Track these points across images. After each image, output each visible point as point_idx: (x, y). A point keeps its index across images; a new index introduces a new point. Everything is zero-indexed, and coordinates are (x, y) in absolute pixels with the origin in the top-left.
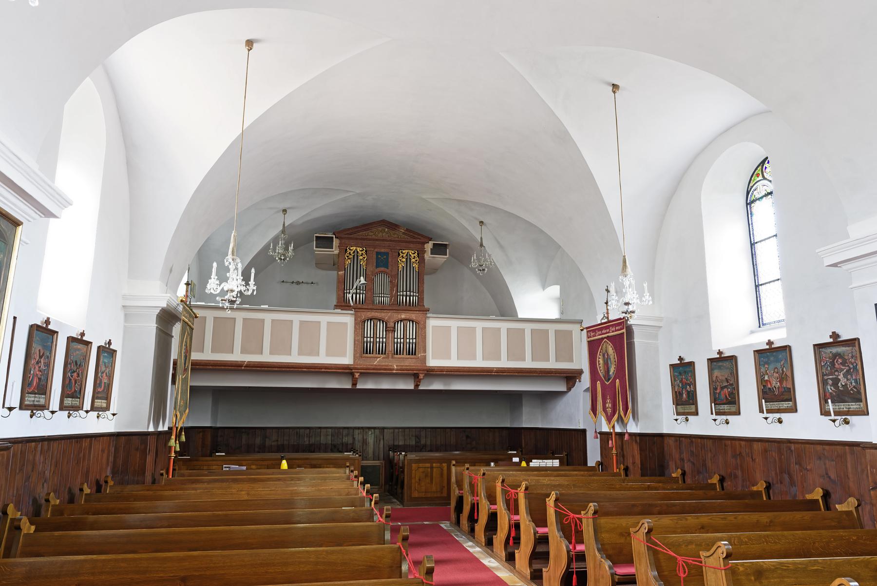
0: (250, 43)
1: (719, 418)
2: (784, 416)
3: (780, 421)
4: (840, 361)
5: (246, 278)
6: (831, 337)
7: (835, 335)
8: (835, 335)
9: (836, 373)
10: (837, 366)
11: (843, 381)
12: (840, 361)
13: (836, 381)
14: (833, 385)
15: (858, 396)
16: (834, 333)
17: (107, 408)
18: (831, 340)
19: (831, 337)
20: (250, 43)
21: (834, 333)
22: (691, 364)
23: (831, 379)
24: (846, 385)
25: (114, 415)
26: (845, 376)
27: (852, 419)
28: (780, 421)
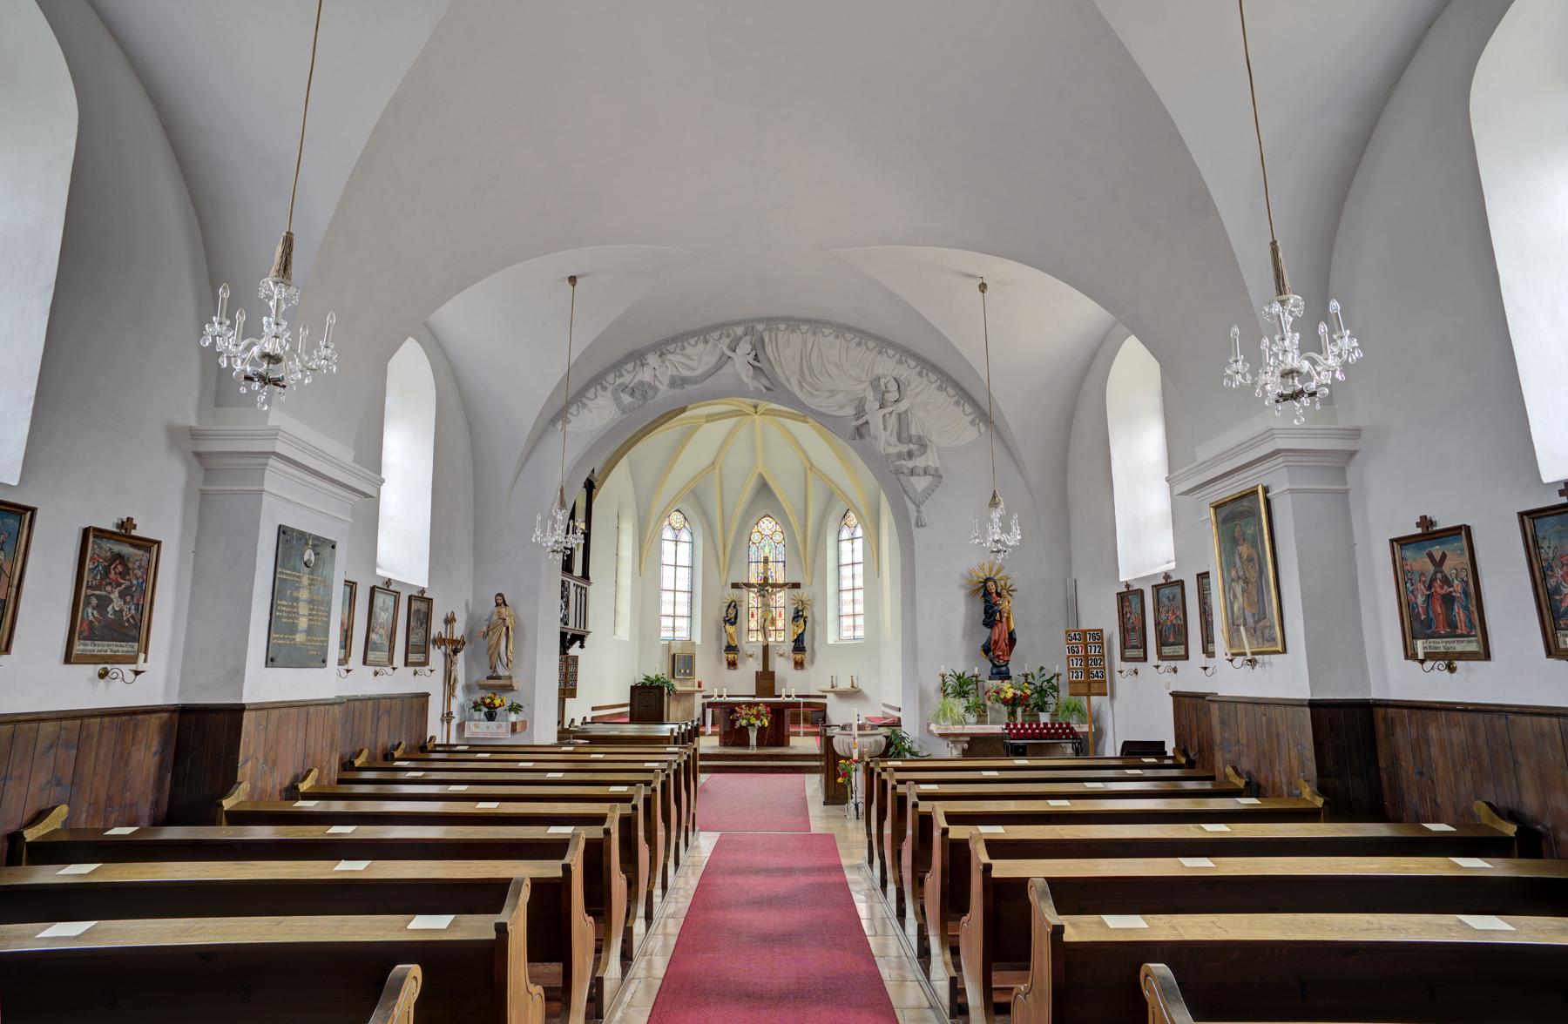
0: (573, 280)
1: (1164, 664)
2: (1179, 664)
3: (1175, 670)
4: (120, 568)
5: (1006, 529)
6: (1418, 525)
7: (1425, 522)
8: (1425, 522)
9: (109, 588)
10: (112, 575)
11: (117, 604)
12: (120, 568)
13: (104, 603)
14: (97, 607)
15: (134, 632)
16: (1424, 518)
17: (426, 663)
18: (1419, 531)
19: (1418, 525)
20: (573, 280)
21: (1424, 518)
22: (1181, 583)
23: (97, 597)
24: (121, 611)
25: (137, 673)
26: (122, 595)
27: (1458, 664)
28: (1175, 670)
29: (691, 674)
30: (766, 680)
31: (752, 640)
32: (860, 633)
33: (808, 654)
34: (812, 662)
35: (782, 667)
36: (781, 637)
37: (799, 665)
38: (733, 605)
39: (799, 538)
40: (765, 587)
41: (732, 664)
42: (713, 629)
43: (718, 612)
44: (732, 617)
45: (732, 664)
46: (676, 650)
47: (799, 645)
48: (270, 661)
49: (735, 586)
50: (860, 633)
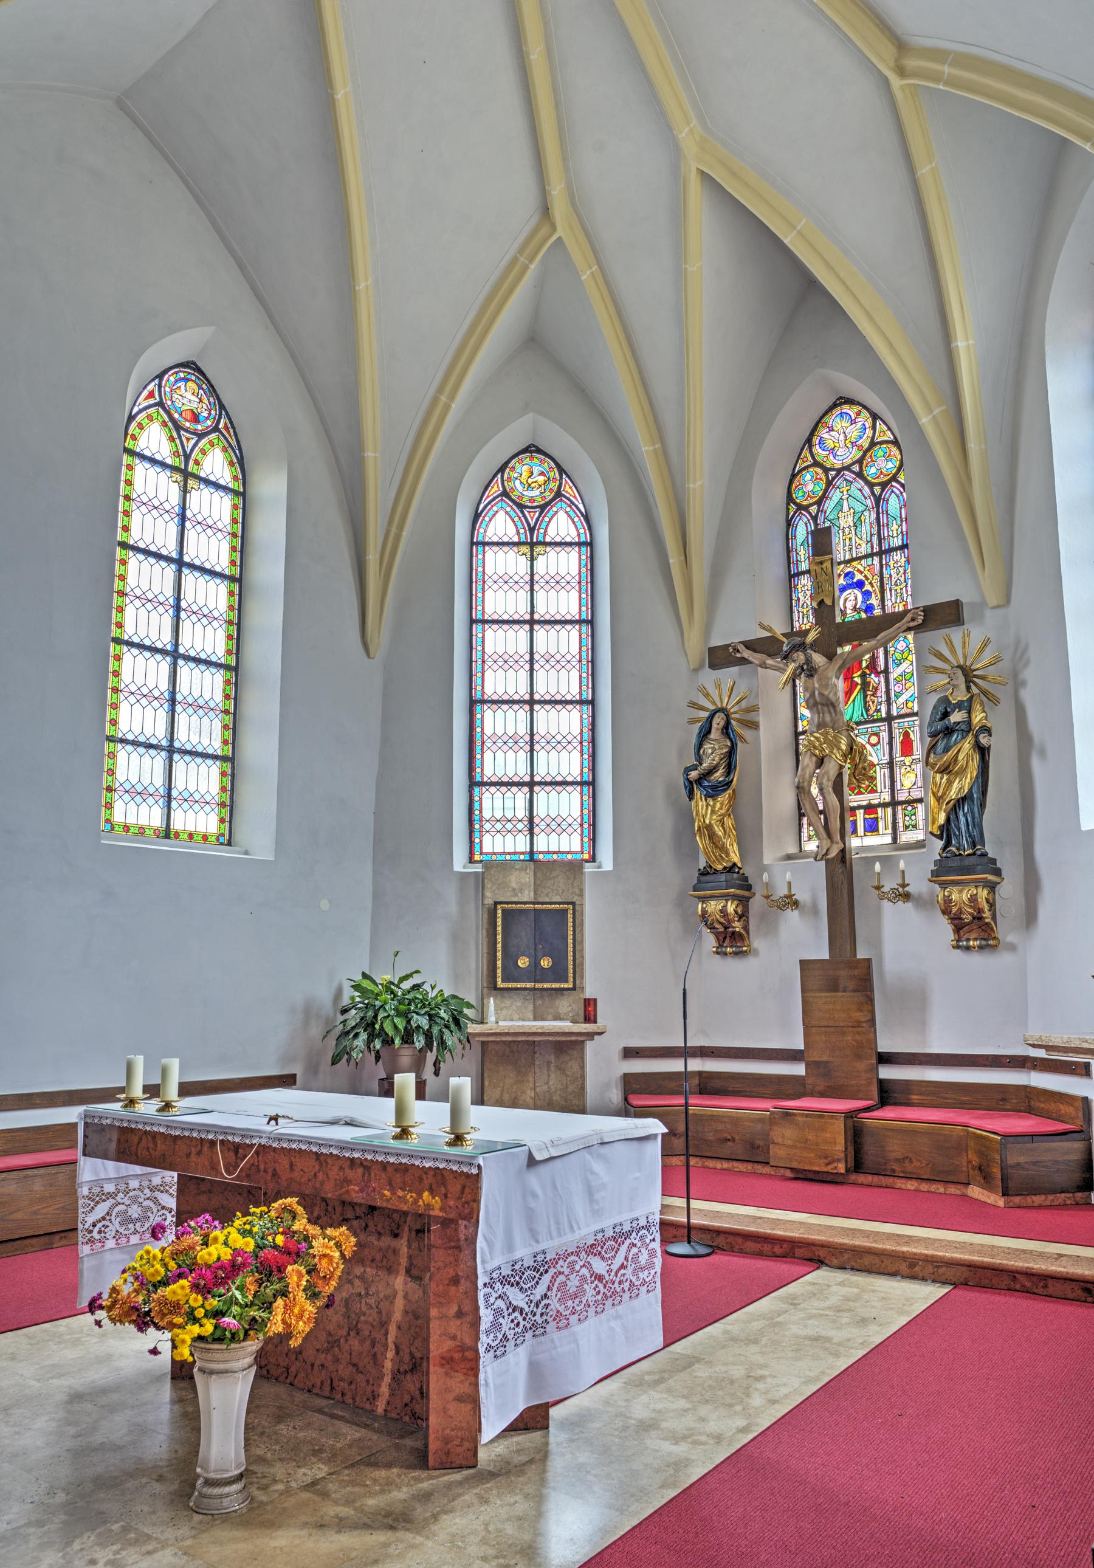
29: (558, 972)
30: (844, 982)
31: (790, 863)
32: (123, 812)
33: (1009, 889)
34: (1030, 917)
35: (907, 941)
36: (899, 837)
37: (974, 929)
38: (727, 728)
39: (929, 420)
40: (838, 642)
41: (732, 939)
42: (665, 820)
43: (672, 751)
44: (716, 769)
45: (732, 939)
46: (521, 889)
47: (962, 851)
48: (595, 1022)
49: (720, 657)
50: (123, 812)
